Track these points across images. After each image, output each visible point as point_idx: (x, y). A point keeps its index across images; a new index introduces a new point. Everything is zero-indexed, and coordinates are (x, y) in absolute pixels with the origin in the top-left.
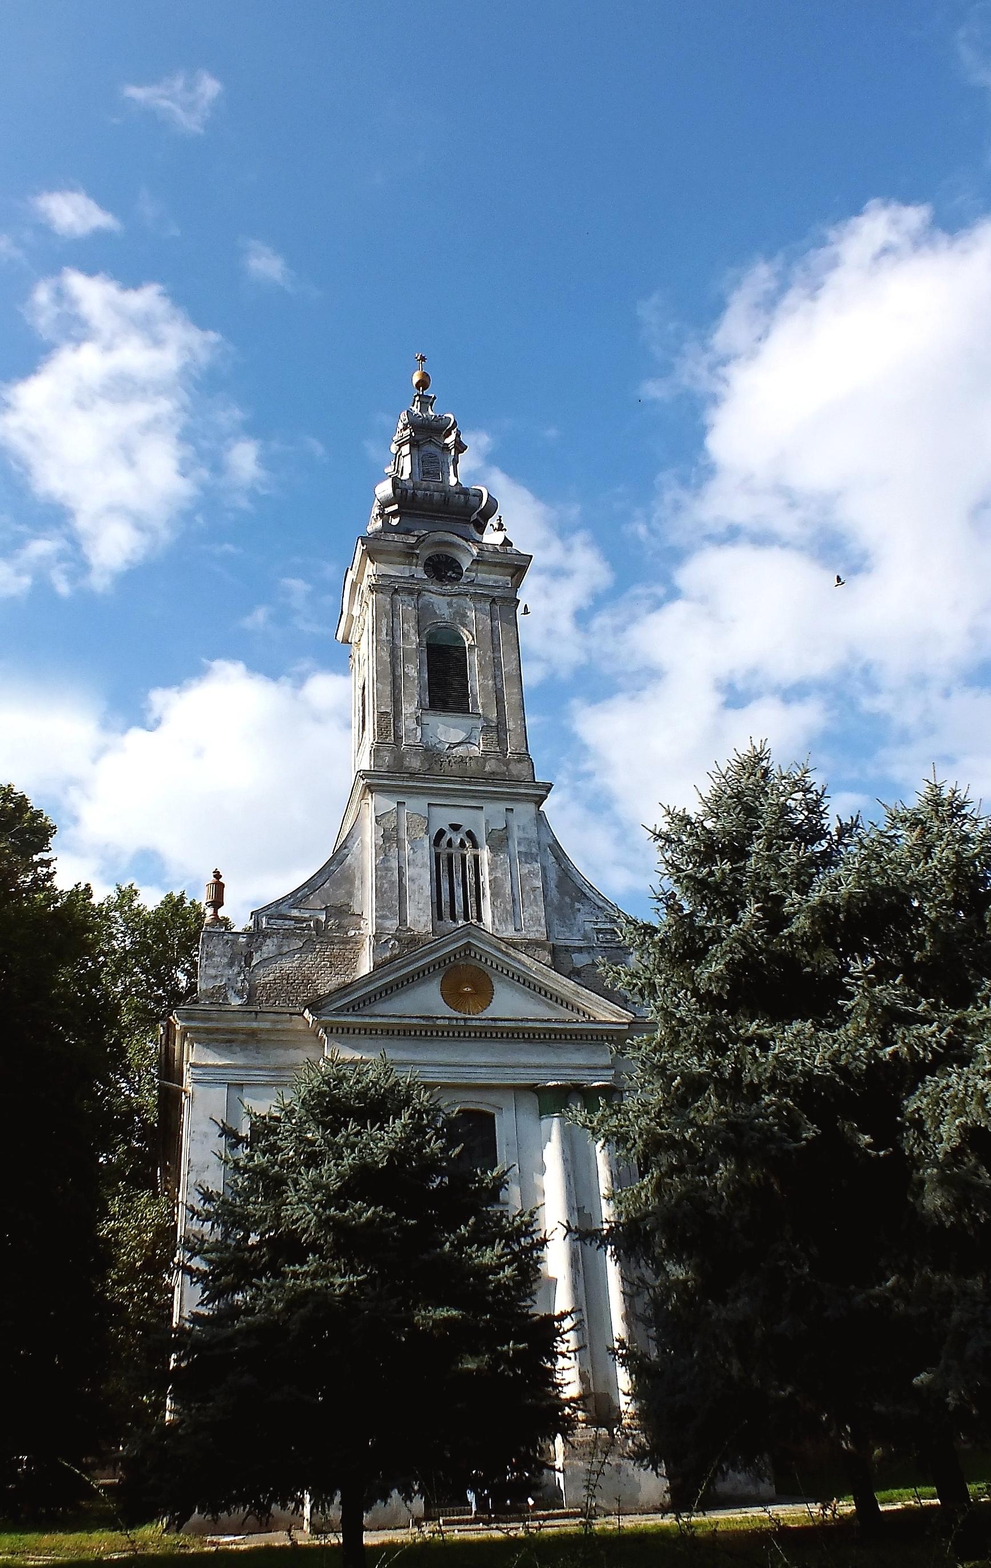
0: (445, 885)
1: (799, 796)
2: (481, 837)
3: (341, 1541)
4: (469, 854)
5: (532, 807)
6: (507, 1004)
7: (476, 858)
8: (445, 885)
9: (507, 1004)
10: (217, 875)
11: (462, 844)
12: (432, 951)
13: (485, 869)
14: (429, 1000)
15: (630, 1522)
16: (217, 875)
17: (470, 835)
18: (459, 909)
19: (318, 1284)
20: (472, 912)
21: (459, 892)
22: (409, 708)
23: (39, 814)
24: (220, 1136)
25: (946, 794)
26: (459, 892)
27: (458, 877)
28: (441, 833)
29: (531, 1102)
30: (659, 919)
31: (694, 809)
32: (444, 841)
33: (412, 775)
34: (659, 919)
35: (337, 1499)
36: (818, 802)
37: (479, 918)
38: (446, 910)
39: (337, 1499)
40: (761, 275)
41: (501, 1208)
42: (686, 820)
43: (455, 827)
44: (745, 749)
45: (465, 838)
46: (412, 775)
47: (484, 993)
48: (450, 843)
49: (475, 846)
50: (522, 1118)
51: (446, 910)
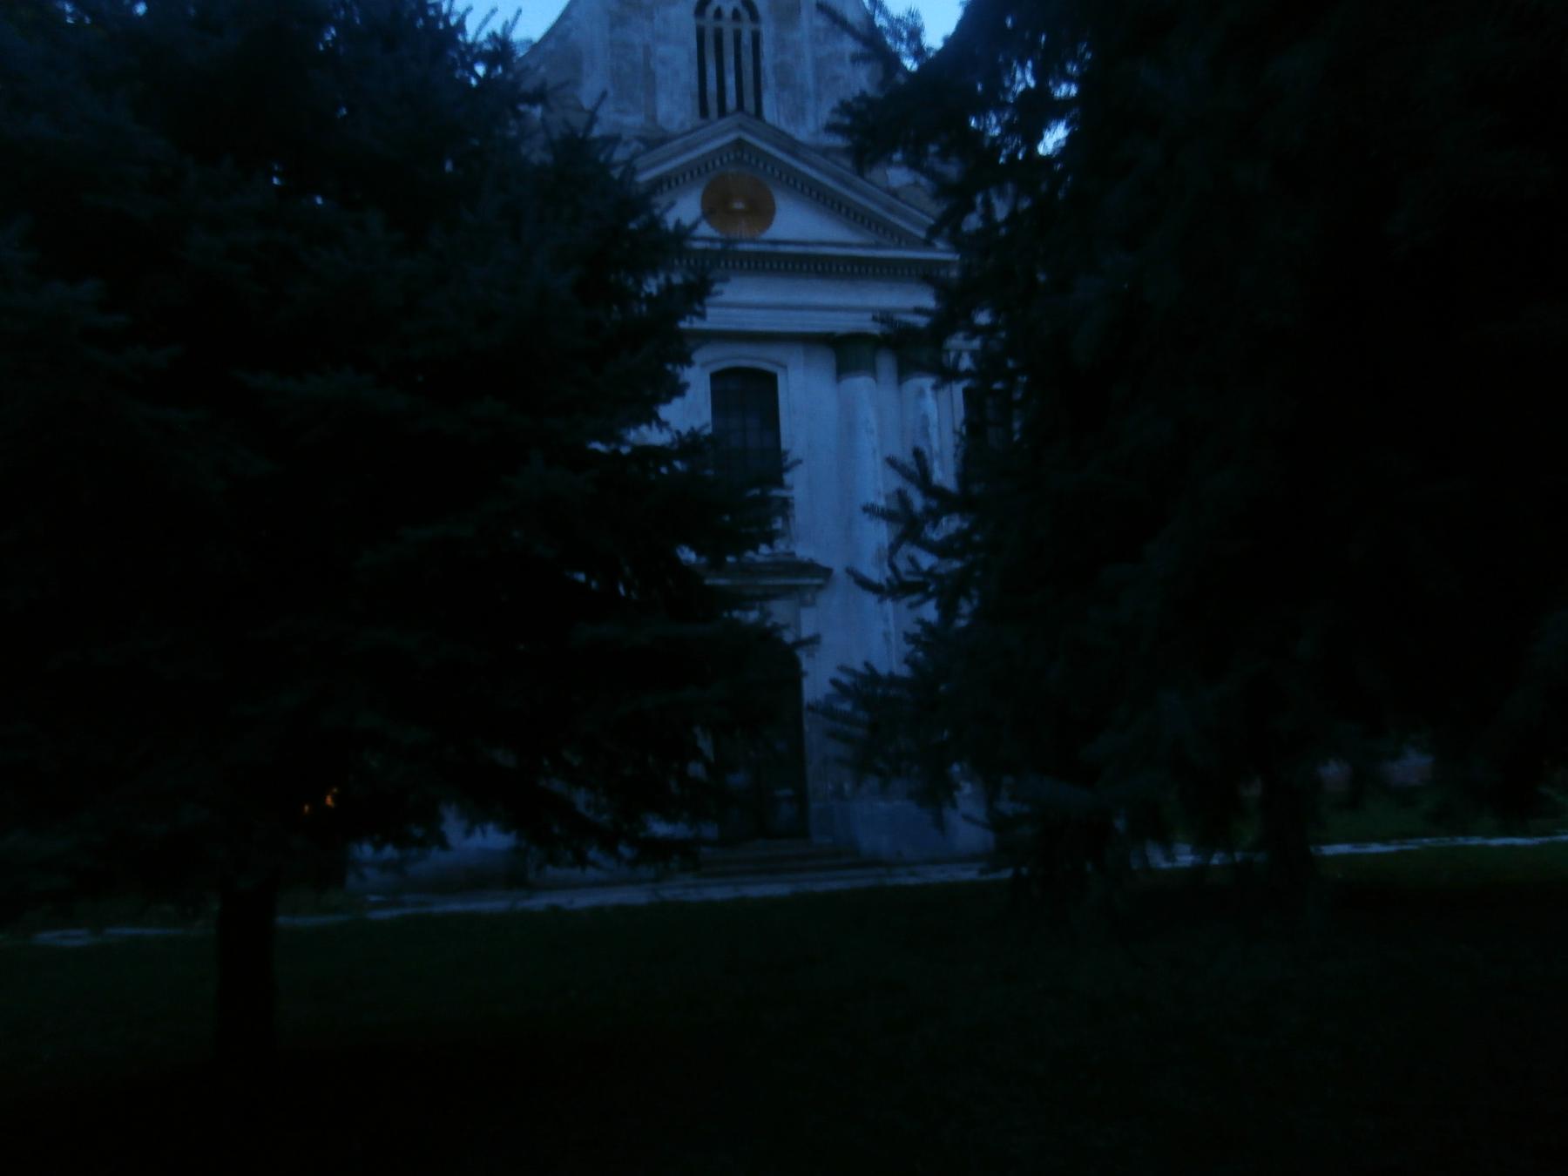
3: (1032, 84)
4: (747, 29)
7: (756, 38)
10: (519, 12)
11: (736, 15)
12: (688, 148)
13: (767, 49)
15: (936, 875)
16: (519, 12)
20: (749, 104)
21: (730, 81)
23: (786, 504)
24: (867, 664)
26: (730, 81)
30: (904, 671)
34: (904, 671)
38: (713, 106)
45: (741, 9)
47: (762, 212)
48: (718, 14)
49: (754, 17)
50: (868, 176)
51: (713, 106)
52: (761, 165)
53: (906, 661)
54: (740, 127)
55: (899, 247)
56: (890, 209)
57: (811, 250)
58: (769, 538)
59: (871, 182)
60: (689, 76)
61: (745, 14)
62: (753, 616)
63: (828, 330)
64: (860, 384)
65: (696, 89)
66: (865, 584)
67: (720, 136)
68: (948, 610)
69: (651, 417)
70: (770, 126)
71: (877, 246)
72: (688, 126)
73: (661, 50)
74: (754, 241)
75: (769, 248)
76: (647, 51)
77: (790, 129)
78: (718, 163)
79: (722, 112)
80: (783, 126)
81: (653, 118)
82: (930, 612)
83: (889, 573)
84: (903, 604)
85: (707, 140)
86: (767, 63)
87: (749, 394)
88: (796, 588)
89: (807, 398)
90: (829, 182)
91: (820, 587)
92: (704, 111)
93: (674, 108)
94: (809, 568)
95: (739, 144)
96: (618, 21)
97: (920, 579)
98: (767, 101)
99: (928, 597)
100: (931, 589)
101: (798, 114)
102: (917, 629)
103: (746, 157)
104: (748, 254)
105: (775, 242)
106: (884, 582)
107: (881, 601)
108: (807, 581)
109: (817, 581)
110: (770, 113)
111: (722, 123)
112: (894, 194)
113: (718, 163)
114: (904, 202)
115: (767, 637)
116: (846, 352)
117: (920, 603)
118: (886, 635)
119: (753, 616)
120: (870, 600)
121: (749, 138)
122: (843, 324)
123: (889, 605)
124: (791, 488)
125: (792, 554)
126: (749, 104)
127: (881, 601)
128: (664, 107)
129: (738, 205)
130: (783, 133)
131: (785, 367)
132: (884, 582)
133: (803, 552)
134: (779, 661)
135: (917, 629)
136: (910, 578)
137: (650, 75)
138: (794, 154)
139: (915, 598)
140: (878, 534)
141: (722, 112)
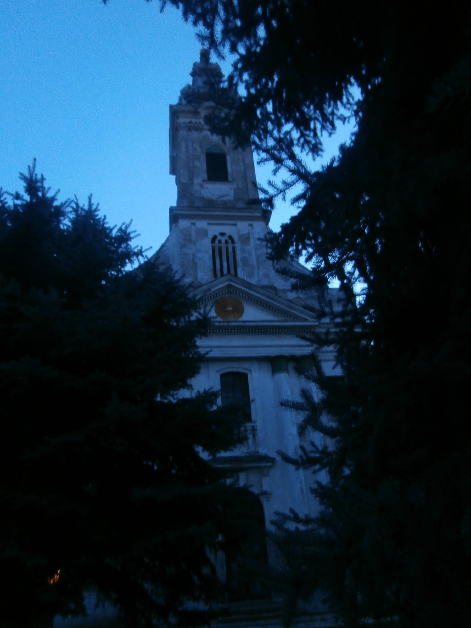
0: (218, 261)
2: (236, 238)
5: (262, 224)
8: (218, 261)
9: (252, 314)
11: (226, 242)
13: (238, 253)
16: (132, 220)
17: (230, 237)
18: (225, 271)
19: (310, 527)
20: (232, 271)
21: (225, 264)
22: (197, 181)
26: (225, 264)
27: (224, 258)
28: (215, 238)
29: (267, 368)
32: (217, 241)
33: (198, 208)
38: (219, 273)
40: (335, 164)
41: (252, 424)
43: (222, 234)
46: (198, 208)
47: (239, 311)
48: (220, 242)
49: (233, 242)
51: (219, 273)
52: (238, 293)
53: (23, 177)
54: (229, 280)
55: (294, 321)
56: (289, 307)
57: (259, 324)
58: (242, 440)
59: (280, 297)
60: (209, 263)
61: (230, 241)
62: (229, 481)
63: (266, 355)
64: (282, 377)
65: (212, 268)
66: (287, 459)
67: (221, 284)
68: (335, 474)
69: (186, 386)
70: (240, 279)
71: (285, 321)
72: (210, 281)
73: (199, 255)
74: (236, 322)
75: (242, 324)
76: (194, 255)
77: (249, 280)
78: (221, 293)
79: (222, 275)
80: (246, 279)
81: (196, 279)
82: (324, 477)
83: (276, 190)
84: (309, 472)
85: (216, 286)
86: (239, 257)
87: (236, 383)
88: (259, 468)
89: (261, 383)
90: (264, 298)
91: (270, 467)
92: (215, 275)
93: (204, 275)
94: (265, 458)
95: (229, 286)
96: (182, 246)
97: (317, 455)
98: (239, 270)
99: (323, 466)
100: (325, 461)
101: (251, 274)
102: (316, 486)
103: (232, 291)
104: (234, 327)
105: (244, 322)
106: (298, 458)
107: (297, 469)
108: (264, 464)
109: (269, 464)
110: (240, 274)
111: (223, 278)
112: (290, 301)
113: (221, 293)
114: (294, 304)
115: (245, 492)
116: (276, 363)
117: (319, 470)
118: (301, 489)
119: (229, 481)
120: (292, 468)
121: (232, 284)
122: (273, 352)
123: (301, 472)
124: (255, 422)
125: (258, 452)
126: (232, 271)
127: (297, 469)
128: (200, 275)
129: (230, 308)
130: (246, 281)
131: (250, 371)
132: (298, 458)
133: (262, 451)
134: (252, 504)
135: (316, 486)
136: (312, 455)
137: (195, 263)
138: (249, 288)
139: (317, 467)
140: (292, 419)
141: (222, 275)
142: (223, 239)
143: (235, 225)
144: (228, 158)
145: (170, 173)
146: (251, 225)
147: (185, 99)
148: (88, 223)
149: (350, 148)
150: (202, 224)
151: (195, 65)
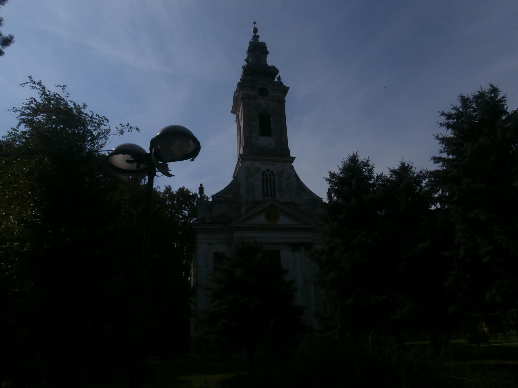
1: (366, 168)
6: (283, 220)
7: (274, 179)
9: (283, 220)
10: (201, 185)
11: (270, 175)
14: (261, 219)
17: (272, 172)
21: (269, 189)
25: (406, 165)
26: (269, 189)
28: (264, 172)
31: (337, 171)
35: (451, 157)
36: (371, 169)
37: (275, 196)
39: (451, 157)
42: (335, 175)
43: (268, 170)
44: (351, 155)
48: (267, 174)
98: (277, 192)
116: (295, 247)
142: (268, 173)
143: (275, 165)
144: (272, 119)
145: (287, 89)
146: (284, 165)
147: (337, 192)
148: (187, 190)
149: (82, 149)
150: (257, 164)
151: (250, 43)
